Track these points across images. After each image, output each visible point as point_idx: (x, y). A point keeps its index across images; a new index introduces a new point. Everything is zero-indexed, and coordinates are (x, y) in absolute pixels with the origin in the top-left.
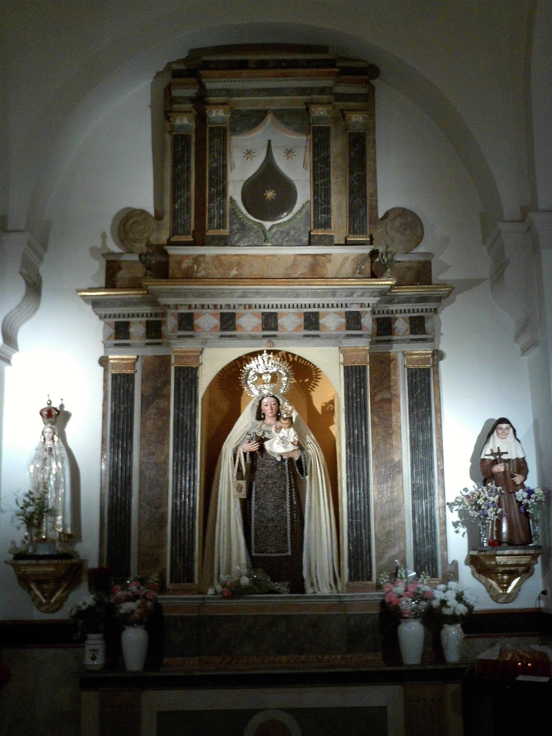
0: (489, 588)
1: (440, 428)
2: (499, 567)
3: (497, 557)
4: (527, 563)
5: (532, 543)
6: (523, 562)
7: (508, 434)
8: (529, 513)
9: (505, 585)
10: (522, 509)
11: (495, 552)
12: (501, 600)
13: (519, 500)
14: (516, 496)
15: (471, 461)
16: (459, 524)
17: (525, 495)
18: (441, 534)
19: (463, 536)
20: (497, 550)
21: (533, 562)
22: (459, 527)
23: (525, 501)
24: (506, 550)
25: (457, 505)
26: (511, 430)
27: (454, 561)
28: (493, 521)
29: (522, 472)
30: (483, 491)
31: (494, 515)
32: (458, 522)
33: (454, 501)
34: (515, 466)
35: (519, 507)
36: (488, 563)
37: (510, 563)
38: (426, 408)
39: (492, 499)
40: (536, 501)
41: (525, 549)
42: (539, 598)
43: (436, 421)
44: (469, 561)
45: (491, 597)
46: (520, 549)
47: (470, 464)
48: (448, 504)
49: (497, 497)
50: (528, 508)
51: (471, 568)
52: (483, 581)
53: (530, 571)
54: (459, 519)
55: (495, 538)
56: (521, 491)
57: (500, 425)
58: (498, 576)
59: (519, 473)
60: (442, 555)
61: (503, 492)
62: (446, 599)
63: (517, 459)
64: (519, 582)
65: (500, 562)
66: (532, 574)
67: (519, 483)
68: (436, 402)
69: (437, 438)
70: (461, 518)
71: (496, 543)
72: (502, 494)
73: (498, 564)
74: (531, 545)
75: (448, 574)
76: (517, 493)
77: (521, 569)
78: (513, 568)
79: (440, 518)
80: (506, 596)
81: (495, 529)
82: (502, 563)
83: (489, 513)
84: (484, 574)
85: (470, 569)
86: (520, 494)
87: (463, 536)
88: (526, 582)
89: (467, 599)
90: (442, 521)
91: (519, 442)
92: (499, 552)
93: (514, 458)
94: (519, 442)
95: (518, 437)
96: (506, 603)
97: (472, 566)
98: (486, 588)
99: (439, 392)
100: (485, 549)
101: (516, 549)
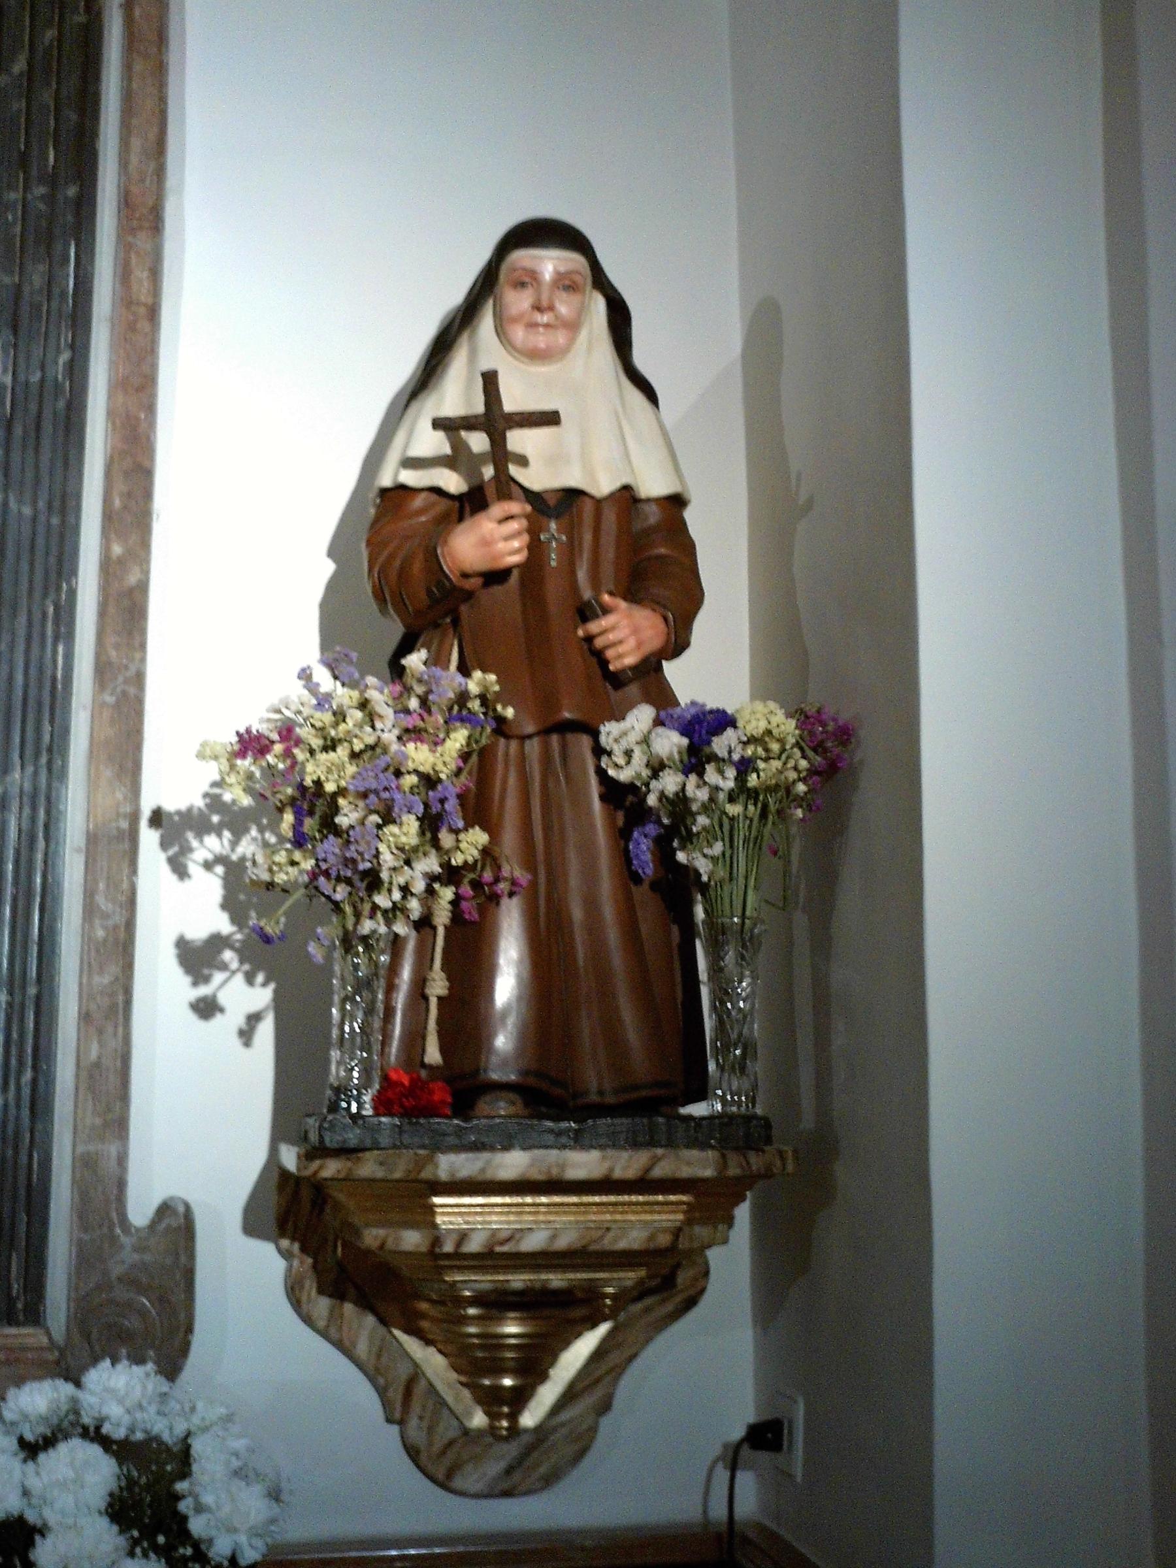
0: (396, 1395)
1: (144, 325)
2: (461, 1269)
3: (437, 1200)
4: (664, 1240)
5: (701, 1095)
6: (633, 1240)
7: (573, 326)
8: (688, 874)
9: (508, 1382)
10: (643, 846)
11: (420, 1164)
12: (469, 1479)
13: (624, 776)
14: (599, 751)
15: (332, 553)
16: (228, 955)
17: (670, 742)
18: (85, 1017)
19: (246, 1035)
20: (438, 1147)
21: (701, 1232)
22: (218, 977)
23: (670, 782)
24: (507, 1148)
25: (218, 830)
26: (599, 305)
27: (165, 1209)
28: (424, 924)
29: (657, 591)
30: (364, 705)
31: (432, 878)
32: (217, 942)
33: (200, 803)
34: (609, 553)
35: (623, 835)
36: (372, 1237)
37: (533, 1243)
38: (53, 181)
39: (419, 756)
40: (742, 791)
41: (652, 1143)
42: (733, 1459)
43: (124, 275)
44: (269, 1218)
45: (413, 1452)
46: (612, 1142)
47: (329, 567)
48: (157, 818)
49: (459, 738)
50: (688, 839)
51: (286, 1255)
52: (362, 1348)
53: (683, 1278)
54: (223, 924)
55: (433, 1055)
56: (641, 717)
57: (522, 257)
58: (466, 1320)
59: (633, 592)
60: (86, 1164)
61: (510, 712)
62: (31, 1517)
63: (627, 496)
64: (598, 1355)
65: (463, 1236)
66: (691, 1303)
67: (630, 661)
68: (134, 159)
69: (118, 385)
70: (237, 918)
71: (440, 1093)
72: (501, 727)
73: (448, 1248)
74: (698, 1109)
75: (121, 1294)
76: (609, 731)
77: (613, 1281)
78: (556, 1280)
79: (90, 910)
80: (512, 1450)
81: (438, 986)
82: (474, 1245)
83: (388, 858)
84: (366, 1304)
85: (280, 1264)
86: (633, 737)
87: (246, 1035)
88: (649, 1354)
89: (200, 1509)
90: (100, 933)
91: (650, 394)
92: (451, 1165)
93: (603, 485)
94: (650, 394)
95: (641, 359)
96: (507, 1494)
97: (285, 1243)
98: (382, 1392)
99: (162, 100)
100: (353, 1137)
101: (578, 1141)
